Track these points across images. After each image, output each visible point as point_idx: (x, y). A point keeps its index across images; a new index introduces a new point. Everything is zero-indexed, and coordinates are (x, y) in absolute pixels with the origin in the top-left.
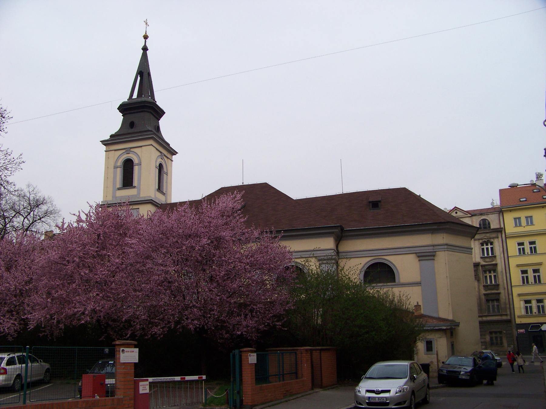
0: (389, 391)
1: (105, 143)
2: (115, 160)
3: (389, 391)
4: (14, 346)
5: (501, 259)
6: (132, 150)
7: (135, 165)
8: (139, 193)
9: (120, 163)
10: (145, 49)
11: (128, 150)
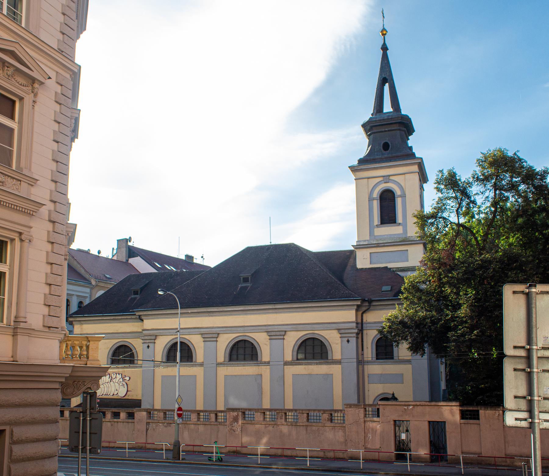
0: (514, 292)
1: (353, 169)
2: (370, 191)
3: (514, 292)
4: (398, 452)
5: (79, 364)
6: (391, 178)
7: (397, 198)
8: (405, 230)
9: (376, 194)
10: (385, 48)
11: (386, 179)
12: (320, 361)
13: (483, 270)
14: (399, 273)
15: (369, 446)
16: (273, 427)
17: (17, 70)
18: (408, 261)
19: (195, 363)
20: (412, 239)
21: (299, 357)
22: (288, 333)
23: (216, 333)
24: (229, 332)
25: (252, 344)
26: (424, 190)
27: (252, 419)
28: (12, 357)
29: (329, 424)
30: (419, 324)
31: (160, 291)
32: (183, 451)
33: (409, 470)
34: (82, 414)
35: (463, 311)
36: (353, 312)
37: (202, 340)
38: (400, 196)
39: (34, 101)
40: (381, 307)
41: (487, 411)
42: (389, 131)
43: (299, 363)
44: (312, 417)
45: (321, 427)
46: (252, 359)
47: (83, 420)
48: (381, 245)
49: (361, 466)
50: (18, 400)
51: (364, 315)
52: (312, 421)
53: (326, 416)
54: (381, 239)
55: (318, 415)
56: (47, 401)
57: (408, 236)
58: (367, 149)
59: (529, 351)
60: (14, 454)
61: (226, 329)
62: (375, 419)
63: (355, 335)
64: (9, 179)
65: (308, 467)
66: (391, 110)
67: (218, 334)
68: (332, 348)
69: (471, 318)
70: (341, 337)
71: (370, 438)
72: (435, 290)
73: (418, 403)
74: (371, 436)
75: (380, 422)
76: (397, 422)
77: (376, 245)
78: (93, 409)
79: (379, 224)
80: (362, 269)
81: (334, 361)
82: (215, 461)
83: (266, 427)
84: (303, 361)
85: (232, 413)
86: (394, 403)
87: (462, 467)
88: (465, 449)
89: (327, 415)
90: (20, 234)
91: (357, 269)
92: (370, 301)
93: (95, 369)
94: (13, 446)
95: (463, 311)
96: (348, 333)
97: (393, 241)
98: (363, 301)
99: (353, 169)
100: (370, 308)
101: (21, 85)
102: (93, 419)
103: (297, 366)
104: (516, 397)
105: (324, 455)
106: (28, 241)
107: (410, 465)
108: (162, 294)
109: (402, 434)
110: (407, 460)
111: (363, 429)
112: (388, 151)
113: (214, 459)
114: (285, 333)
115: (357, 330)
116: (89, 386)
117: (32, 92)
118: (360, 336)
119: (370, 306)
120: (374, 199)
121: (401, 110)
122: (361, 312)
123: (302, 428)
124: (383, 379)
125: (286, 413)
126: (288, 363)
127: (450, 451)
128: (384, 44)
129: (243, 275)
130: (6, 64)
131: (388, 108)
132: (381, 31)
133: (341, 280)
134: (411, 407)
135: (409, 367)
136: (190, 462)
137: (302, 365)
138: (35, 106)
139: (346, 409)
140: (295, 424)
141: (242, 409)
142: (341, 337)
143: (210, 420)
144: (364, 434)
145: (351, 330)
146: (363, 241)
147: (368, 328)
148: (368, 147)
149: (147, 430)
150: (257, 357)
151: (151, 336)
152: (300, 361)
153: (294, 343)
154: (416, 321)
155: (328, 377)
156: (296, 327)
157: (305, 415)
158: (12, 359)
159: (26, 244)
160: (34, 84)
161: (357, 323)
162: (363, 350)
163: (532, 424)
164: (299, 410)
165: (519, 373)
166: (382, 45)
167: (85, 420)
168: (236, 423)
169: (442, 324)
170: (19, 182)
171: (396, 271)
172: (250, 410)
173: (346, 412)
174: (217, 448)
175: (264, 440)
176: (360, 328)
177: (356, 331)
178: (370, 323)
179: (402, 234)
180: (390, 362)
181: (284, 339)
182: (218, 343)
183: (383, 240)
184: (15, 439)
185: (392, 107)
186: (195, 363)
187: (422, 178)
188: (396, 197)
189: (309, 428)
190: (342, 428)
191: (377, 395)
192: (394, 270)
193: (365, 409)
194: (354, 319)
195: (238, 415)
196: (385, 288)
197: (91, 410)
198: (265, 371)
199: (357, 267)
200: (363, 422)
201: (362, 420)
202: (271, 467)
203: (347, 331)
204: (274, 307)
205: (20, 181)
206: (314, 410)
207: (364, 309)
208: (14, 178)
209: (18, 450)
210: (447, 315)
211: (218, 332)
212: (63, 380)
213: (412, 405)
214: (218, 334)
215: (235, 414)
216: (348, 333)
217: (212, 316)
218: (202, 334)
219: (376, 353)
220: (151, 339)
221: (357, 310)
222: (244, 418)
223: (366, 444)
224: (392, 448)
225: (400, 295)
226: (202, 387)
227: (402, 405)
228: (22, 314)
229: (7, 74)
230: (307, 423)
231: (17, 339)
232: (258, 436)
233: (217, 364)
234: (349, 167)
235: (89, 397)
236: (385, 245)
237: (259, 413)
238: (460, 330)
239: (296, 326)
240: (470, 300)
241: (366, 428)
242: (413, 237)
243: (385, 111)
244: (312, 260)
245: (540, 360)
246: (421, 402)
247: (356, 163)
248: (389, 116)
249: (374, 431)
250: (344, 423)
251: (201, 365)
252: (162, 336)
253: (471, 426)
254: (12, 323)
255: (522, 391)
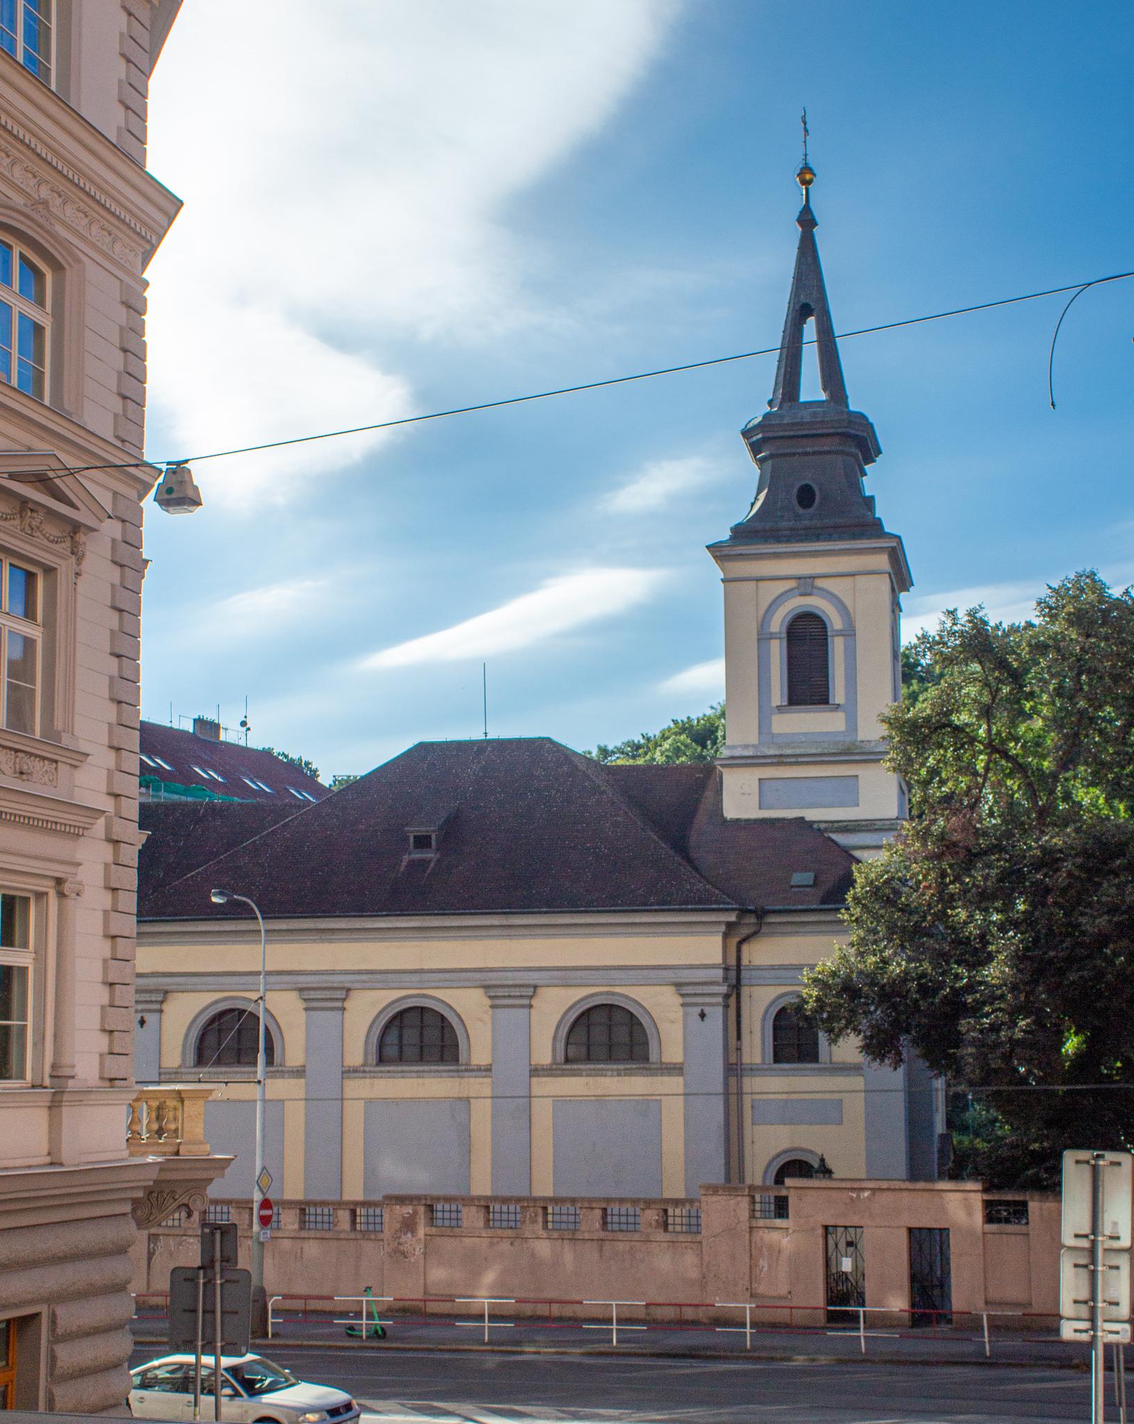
0: (1078, 1162)
2: (761, 612)
3: (1078, 1162)
6: (820, 583)
7: (833, 636)
9: (778, 623)
11: (806, 584)
12: (629, 1066)
13: (1045, 870)
14: (834, 836)
15: (761, 1289)
16: (512, 1244)
17: (51, 512)
18: (858, 805)
19: (280, 1068)
20: (868, 748)
21: (571, 1055)
22: (541, 991)
23: (342, 988)
24: (379, 985)
25: (443, 1018)
26: (901, 611)
27: (454, 1223)
28: (49, 1154)
29: (660, 1236)
30: (890, 994)
31: (215, 895)
32: (276, 1312)
33: (863, 1350)
34: (201, 1272)
35: (995, 972)
36: (718, 940)
37: (302, 1005)
38: (840, 633)
39: (77, 574)
40: (789, 929)
41: (1047, 1204)
42: (814, 453)
43: (572, 1070)
44: (616, 1219)
45: (638, 1244)
46: (442, 1060)
47: (205, 1284)
48: (788, 760)
49: (748, 1343)
50: (64, 1247)
51: (745, 948)
52: (616, 1227)
53: (652, 1215)
54: (788, 745)
55: (631, 1212)
56: (113, 1243)
57: (859, 739)
58: (756, 499)
59: (1094, 1243)
60: (59, 1364)
61: (370, 976)
62: (779, 1222)
63: (720, 1000)
64: (38, 764)
65: (616, 1347)
66: (823, 396)
67: (349, 990)
68: (660, 1030)
69: (1014, 988)
70: (683, 1005)
71: (765, 1269)
72: (929, 905)
73: (884, 1185)
74: (766, 1265)
75: (790, 1231)
76: (831, 1229)
77: (774, 760)
78: (228, 1261)
79: (785, 703)
80: (738, 820)
81: (664, 1066)
82: (368, 1337)
83: (492, 1245)
84: (581, 1067)
85: (398, 1207)
86: (825, 1183)
87: (986, 1340)
88: (994, 1295)
89: (655, 1212)
90: (59, 881)
91: (725, 820)
92: (761, 914)
93: (198, 1165)
94: (55, 1347)
95: (995, 972)
96: (704, 995)
97: (819, 751)
98: (743, 912)
99: (718, 554)
100: (759, 931)
101: (52, 541)
102: (227, 1281)
103: (566, 1079)
104: (1076, 1302)
105: (648, 1314)
106: (74, 895)
107: (865, 1337)
108: (221, 901)
109: (844, 1259)
110: (859, 1322)
111: (748, 1248)
112: (811, 510)
113: (364, 1333)
114: (534, 992)
115: (725, 988)
116: (185, 1201)
117: (73, 553)
118: (733, 1001)
119: (760, 925)
120: (772, 636)
121: (847, 397)
122: (734, 941)
123: (589, 1244)
124: (789, 1112)
125: (545, 1209)
126: (543, 1070)
127: (958, 1301)
128: (806, 210)
129: (413, 831)
130: (30, 505)
131: (812, 389)
132: (798, 171)
133: (681, 846)
134: (866, 1194)
135: (858, 1082)
136: (299, 1343)
137: (581, 1075)
138: (78, 582)
139: (703, 1198)
140: (570, 1234)
141: (426, 1197)
142: (683, 1005)
143: (336, 1225)
144: (747, 1260)
145: (711, 987)
146: (740, 746)
147: (754, 982)
148: (758, 493)
149: (150, 1255)
150: (458, 1053)
151: (150, 991)
152: (575, 1067)
153: (559, 1016)
154: (884, 986)
155: (649, 1107)
156: (565, 975)
157: (598, 1213)
158: (48, 1160)
159: (70, 903)
160: (78, 535)
161: (726, 969)
162: (739, 1037)
163: (1094, 1337)
164: (583, 1199)
165: (1081, 1270)
166: (801, 212)
167: (209, 1283)
168: (409, 1235)
169: (945, 997)
170: (54, 764)
171: (826, 830)
172: (448, 1199)
173: (703, 1204)
174: (373, 1304)
175: (490, 1277)
176: (734, 982)
177: (723, 989)
178: (758, 968)
179: (843, 732)
180: (808, 1069)
181: (531, 1006)
182: (347, 1014)
183: (793, 748)
184: (59, 1331)
185: (824, 390)
186: (280, 1068)
187: (897, 581)
188: (829, 634)
189: (607, 1245)
190: (694, 1246)
191: (774, 1152)
192: (823, 826)
193: (753, 1197)
194: (718, 958)
195: (415, 1212)
196: (800, 878)
197: (224, 1264)
198: (479, 1087)
199: (725, 815)
200: (748, 1230)
201: (745, 1226)
202: (519, 1349)
203: (699, 990)
204: (504, 922)
205: (56, 762)
206: (622, 1201)
207: (745, 931)
208: (44, 758)
209: (69, 1356)
210: (958, 977)
211: (347, 985)
212: (140, 1194)
213: (870, 1189)
214: (349, 990)
215: (409, 1210)
216: (704, 995)
217: (330, 941)
218: (301, 990)
219: (775, 1047)
220: (152, 1002)
221: (726, 936)
222: (431, 1221)
223: (754, 1285)
224: (818, 1297)
225: (843, 911)
226: (360, 1164)
227: (845, 1189)
228: (66, 1060)
229: (30, 525)
230: (602, 1234)
231: (60, 1115)
232: (474, 1264)
233: (343, 1073)
234: (708, 547)
235: (218, 1236)
236: (800, 760)
237: (474, 1209)
238: (987, 1015)
239: (563, 973)
240: (1013, 944)
241: (753, 1244)
242: (873, 744)
243: (803, 398)
244: (604, 792)
245: (1107, 1254)
246: (891, 1182)
247: (725, 535)
248: (815, 414)
249: (775, 1251)
250: (699, 1233)
251: (299, 1072)
252: (183, 992)
253: (1008, 1238)
254: (47, 1082)
255: (1084, 1294)
